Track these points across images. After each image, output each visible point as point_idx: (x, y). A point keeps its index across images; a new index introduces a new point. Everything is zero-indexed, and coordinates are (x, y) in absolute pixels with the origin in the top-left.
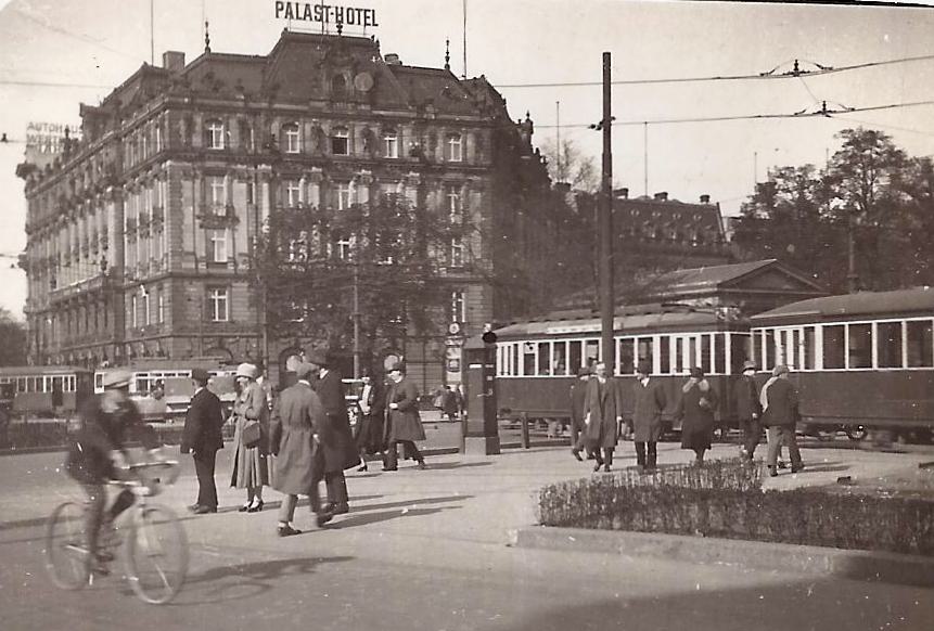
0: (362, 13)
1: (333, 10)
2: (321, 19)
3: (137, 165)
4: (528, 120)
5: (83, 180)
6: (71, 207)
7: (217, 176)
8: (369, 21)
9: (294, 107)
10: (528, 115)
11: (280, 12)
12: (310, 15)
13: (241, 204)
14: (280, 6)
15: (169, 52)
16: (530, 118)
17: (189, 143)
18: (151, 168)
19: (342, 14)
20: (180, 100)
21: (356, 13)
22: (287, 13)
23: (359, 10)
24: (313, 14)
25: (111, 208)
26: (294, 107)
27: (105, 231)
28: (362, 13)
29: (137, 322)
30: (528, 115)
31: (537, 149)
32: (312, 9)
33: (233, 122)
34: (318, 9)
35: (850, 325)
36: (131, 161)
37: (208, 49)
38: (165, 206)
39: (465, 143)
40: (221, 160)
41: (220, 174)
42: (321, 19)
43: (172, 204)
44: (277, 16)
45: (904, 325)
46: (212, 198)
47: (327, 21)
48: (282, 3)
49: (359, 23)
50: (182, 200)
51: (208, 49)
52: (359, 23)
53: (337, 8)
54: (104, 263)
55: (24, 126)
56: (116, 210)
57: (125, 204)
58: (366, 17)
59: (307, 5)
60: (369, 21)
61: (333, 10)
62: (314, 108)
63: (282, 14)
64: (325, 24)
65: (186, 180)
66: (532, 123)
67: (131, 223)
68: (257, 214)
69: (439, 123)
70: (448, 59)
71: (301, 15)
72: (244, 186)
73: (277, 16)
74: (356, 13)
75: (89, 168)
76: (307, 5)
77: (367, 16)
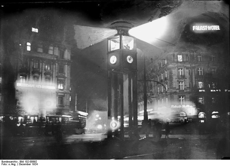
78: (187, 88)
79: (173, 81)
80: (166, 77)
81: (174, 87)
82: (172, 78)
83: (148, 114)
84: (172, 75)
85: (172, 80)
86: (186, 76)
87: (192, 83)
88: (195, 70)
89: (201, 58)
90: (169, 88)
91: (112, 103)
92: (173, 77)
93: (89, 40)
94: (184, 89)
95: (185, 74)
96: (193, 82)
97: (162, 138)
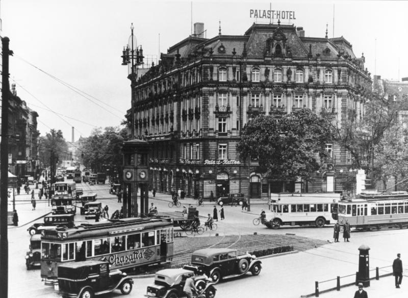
0: (289, 13)
1: (275, 13)
2: (270, 18)
3: (188, 86)
4: (363, 57)
5: (161, 88)
6: (156, 100)
7: (223, 93)
8: (292, 17)
9: (258, 60)
10: (363, 54)
11: (252, 15)
12: (265, 16)
13: (234, 107)
14: (252, 12)
15: (197, 23)
16: (364, 55)
17: (212, 79)
18: (195, 89)
19: (279, 15)
20: (209, 59)
21: (286, 13)
22: (255, 15)
23: (287, 12)
24: (267, 15)
25: (175, 104)
26: (258, 60)
27: (172, 114)
28: (289, 13)
29: (199, 157)
30: (363, 54)
31: (366, 69)
32: (266, 12)
33: (231, 69)
34: (269, 13)
35: (88, 242)
36: (184, 84)
37: (220, 34)
38: (201, 107)
39: (333, 74)
40: (226, 86)
41: (225, 92)
42: (270, 18)
43: (204, 107)
44: (251, 17)
45: (50, 245)
46: (221, 104)
47: (273, 18)
48: (253, 10)
49: (287, 18)
50: (209, 105)
51: (220, 34)
52: (287, 18)
53: (277, 11)
54: (172, 129)
55: (345, 243)
56: (177, 105)
57: (182, 103)
58: (291, 15)
59: (264, 11)
60: (292, 17)
61: (275, 13)
62: (267, 61)
63: (253, 15)
64: (272, 19)
65: (210, 96)
66: (364, 58)
67: (184, 112)
68: (240, 110)
69: (322, 65)
70: (327, 33)
71: (261, 16)
72: (235, 98)
73: (251, 17)
74: (286, 13)
75: (164, 83)
76: (264, 11)
77: (291, 14)
78: (233, 129)
79: (208, 117)
80: (198, 107)
81: (211, 127)
82: (208, 110)
83: (8, 223)
84: (208, 106)
85: (208, 114)
86: (231, 107)
87: (241, 121)
88: (165, 87)
89: (239, 73)
90: (201, 128)
91: (21, 161)
92: (209, 109)
93: (382, 118)
94: (228, 131)
95: (230, 105)
96: (177, 122)
97: (111, 276)
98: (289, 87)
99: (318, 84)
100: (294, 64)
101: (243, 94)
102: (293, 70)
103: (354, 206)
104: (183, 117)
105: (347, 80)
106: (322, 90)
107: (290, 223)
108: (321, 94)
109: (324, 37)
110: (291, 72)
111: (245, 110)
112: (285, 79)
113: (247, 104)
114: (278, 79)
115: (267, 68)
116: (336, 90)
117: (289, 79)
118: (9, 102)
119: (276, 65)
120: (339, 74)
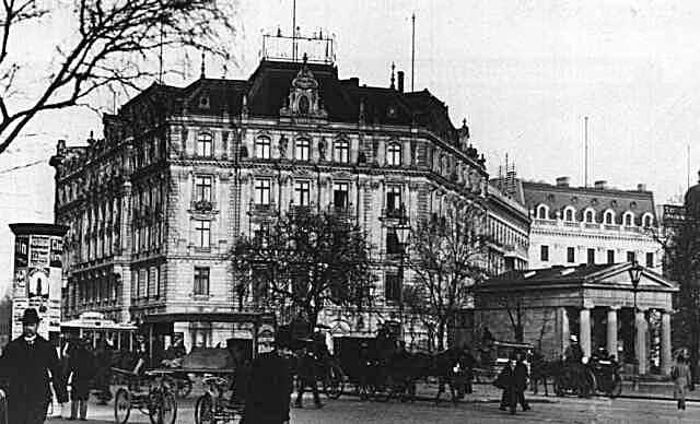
4: (464, 126)
16: (467, 124)
37: (203, 75)
51: (203, 75)
98: (377, 131)
99: (375, 165)
100: (332, 130)
101: (239, 180)
102: (329, 141)
103: (627, 314)
104: (55, 389)
105: (429, 163)
106: (382, 177)
107: (649, 291)
108: (381, 184)
109: (388, 87)
110: (327, 144)
111: (245, 208)
112: (316, 156)
113: (247, 197)
114: (301, 154)
115: (283, 135)
116: (407, 178)
117: (322, 155)
118: (47, 339)
119: (300, 131)
120: (413, 150)
